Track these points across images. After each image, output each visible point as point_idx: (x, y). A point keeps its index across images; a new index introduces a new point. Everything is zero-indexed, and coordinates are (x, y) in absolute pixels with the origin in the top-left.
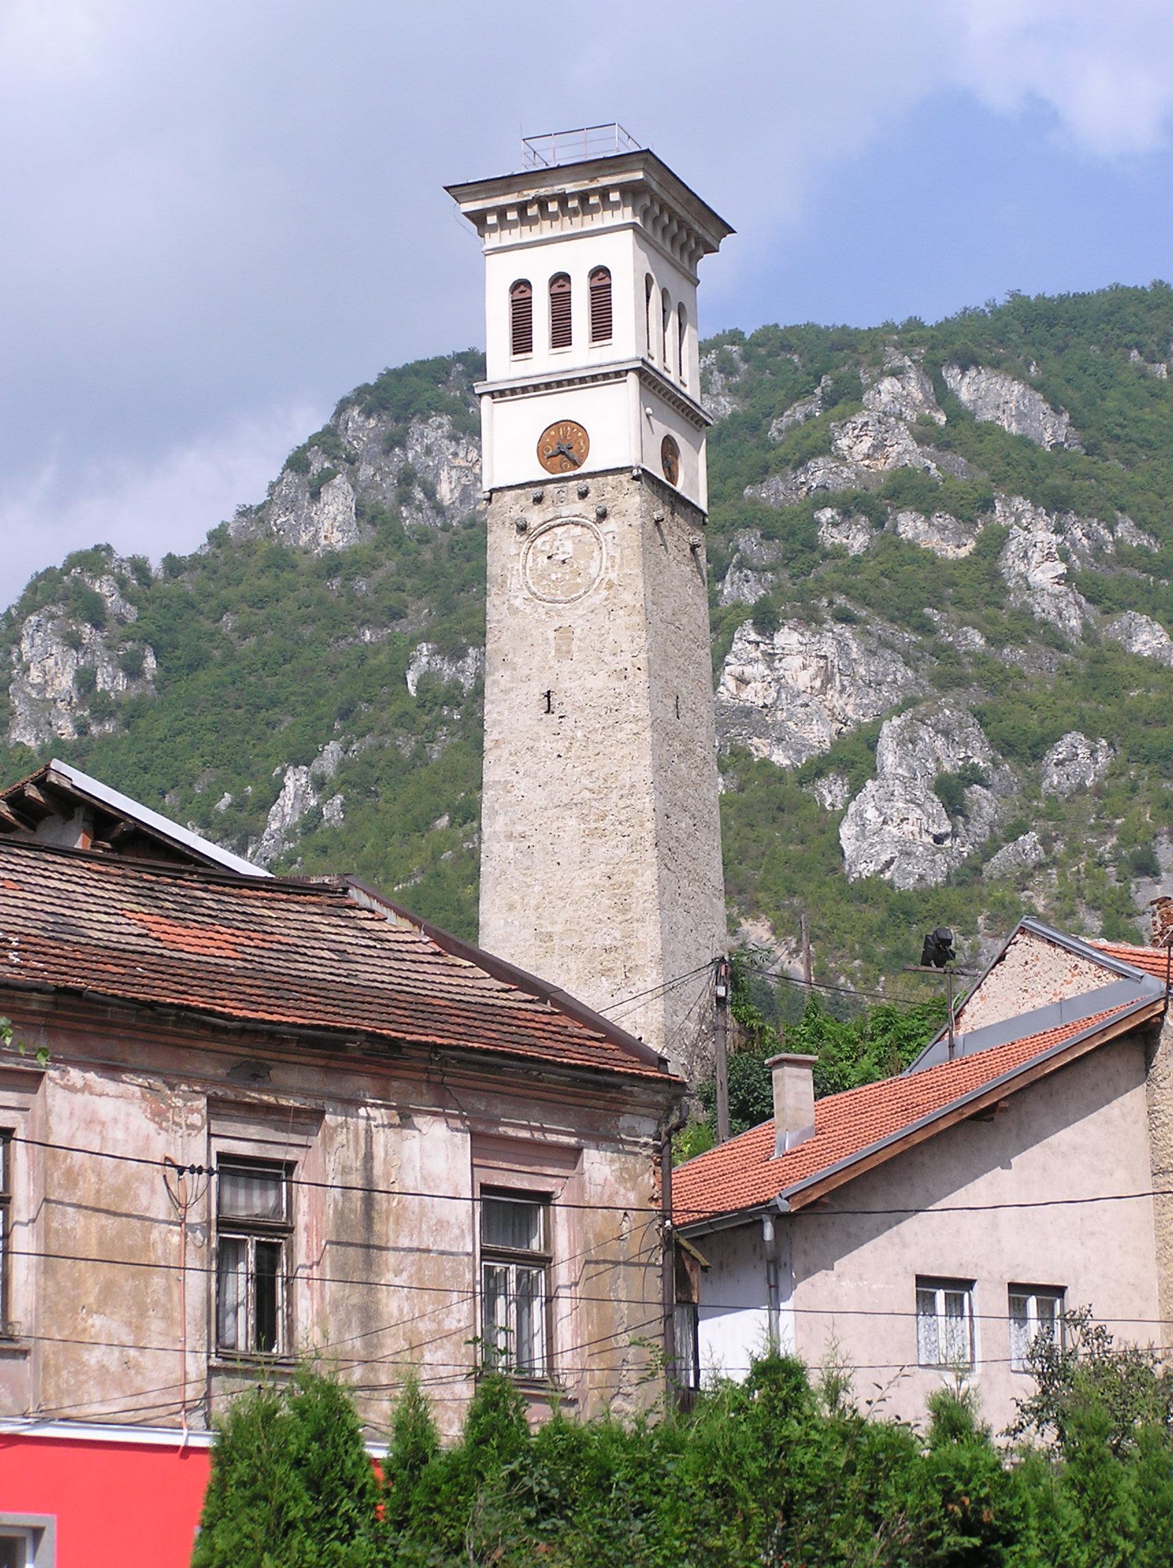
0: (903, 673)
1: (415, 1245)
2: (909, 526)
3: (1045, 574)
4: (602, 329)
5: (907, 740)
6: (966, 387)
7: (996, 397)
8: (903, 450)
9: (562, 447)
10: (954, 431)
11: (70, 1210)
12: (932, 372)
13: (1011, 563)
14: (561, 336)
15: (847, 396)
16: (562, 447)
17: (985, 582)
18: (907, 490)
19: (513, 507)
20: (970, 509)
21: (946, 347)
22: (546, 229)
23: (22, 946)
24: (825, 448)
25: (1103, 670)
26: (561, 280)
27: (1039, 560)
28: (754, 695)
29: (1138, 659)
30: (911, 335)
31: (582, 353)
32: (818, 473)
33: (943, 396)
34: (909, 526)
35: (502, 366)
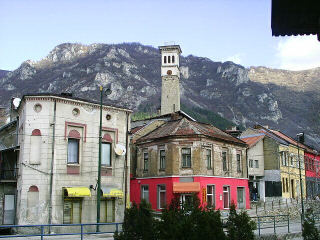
0: (113, 78)
1: (97, 173)
2: (114, 64)
3: (127, 70)
4: (173, 62)
5: (114, 85)
6: (120, 51)
7: (123, 52)
8: (114, 57)
9: (169, 72)
10: (119, 55)
11: (47, 213)
12: (116, 49)
13: (124, 69)
14: (169, 62)
15: (108, 51)
16: (169, 72)
17: (121, 70)
18: (114, 60)
19: (164, 78)
20: (120, 62)
21: (117, 47)
22: (167, 52)
23: (285, 180)
24: (106, 55)
25: (133, 80)
26: (169, 57)
27: (127, 68)
28: (99, 80)
29: (135, 79)
30: (114, 45)
31: (171, 64)
32: (105, 58)
33: (117, 51)
34: (114, 64)
35: (163, 64)
